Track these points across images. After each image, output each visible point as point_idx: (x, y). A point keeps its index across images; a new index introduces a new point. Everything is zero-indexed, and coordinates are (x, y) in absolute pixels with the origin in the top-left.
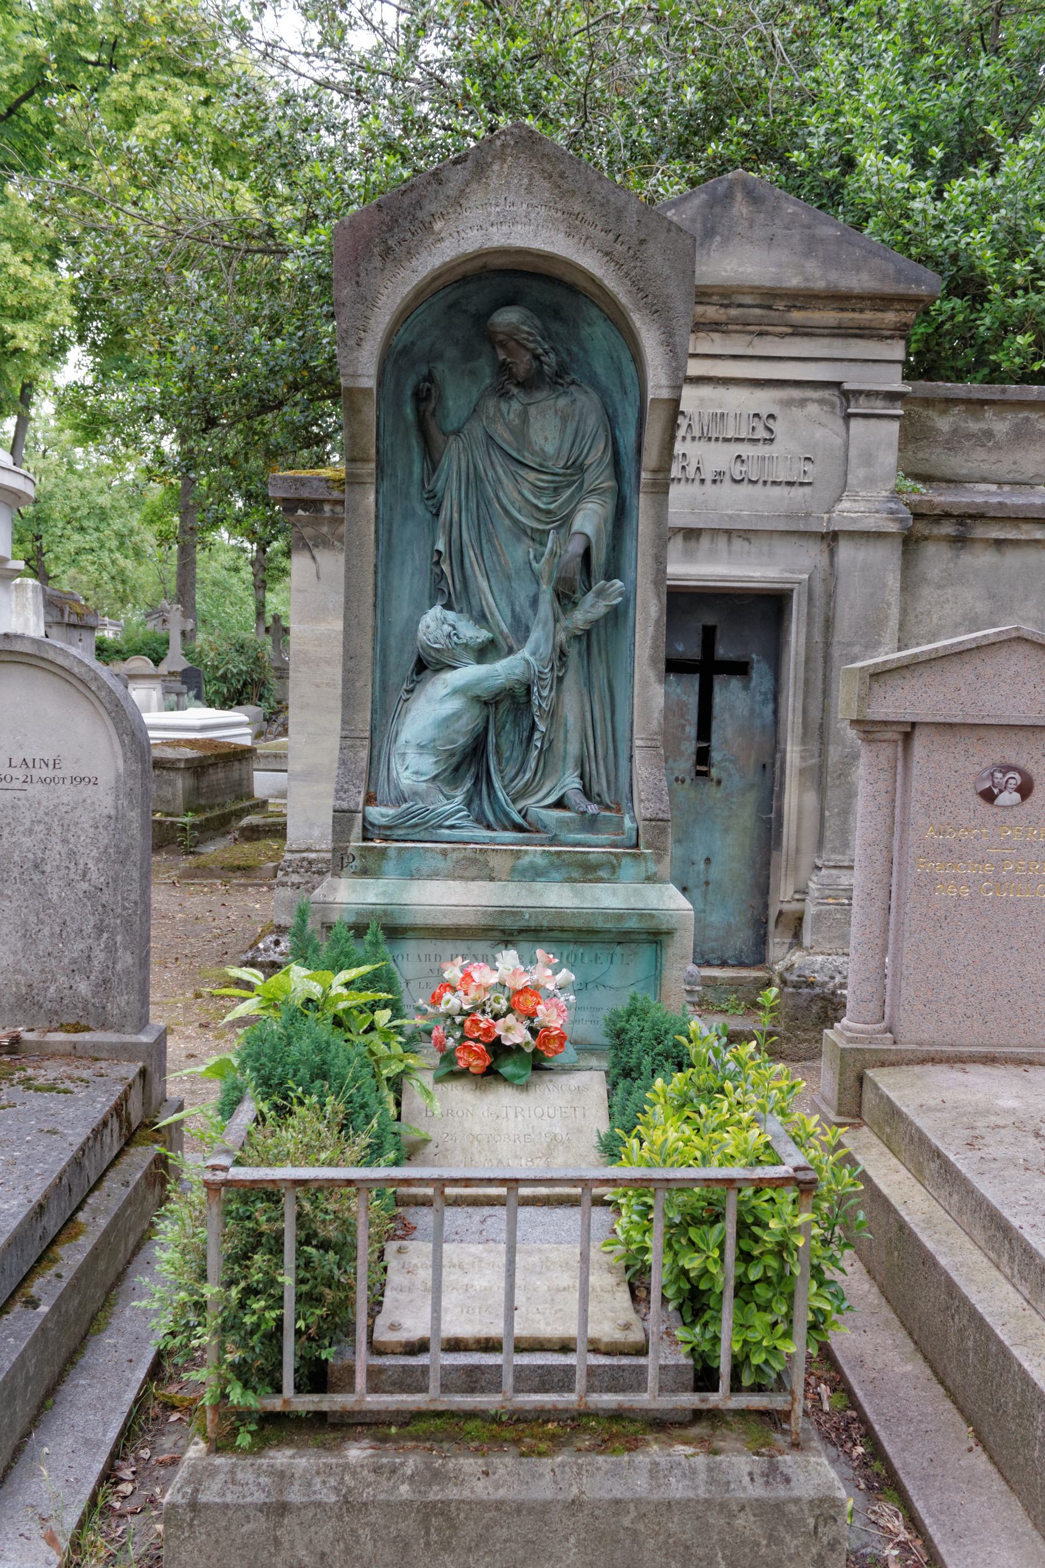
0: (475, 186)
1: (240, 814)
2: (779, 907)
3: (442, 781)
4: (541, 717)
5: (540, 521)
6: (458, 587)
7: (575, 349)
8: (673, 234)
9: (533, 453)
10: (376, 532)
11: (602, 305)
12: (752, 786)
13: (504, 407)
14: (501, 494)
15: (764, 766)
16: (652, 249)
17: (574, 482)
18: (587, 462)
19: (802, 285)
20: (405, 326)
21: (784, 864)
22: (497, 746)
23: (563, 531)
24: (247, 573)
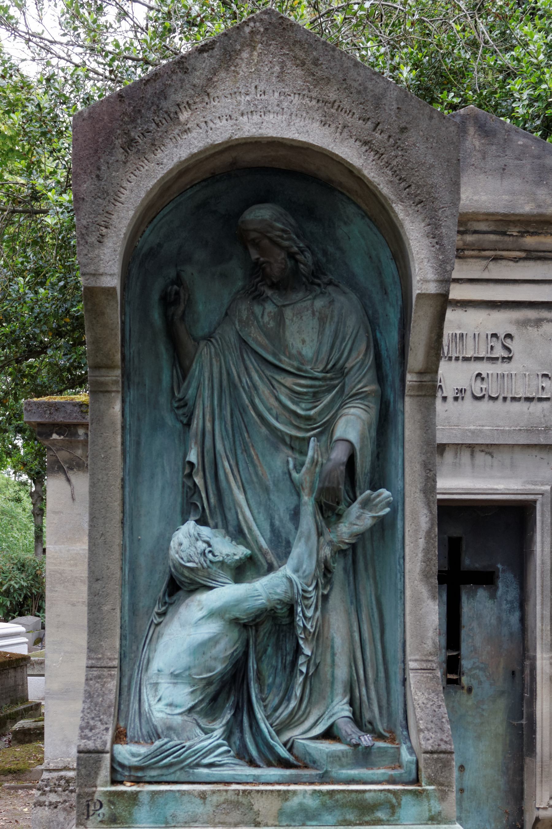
0: (223, 74)
1: (15, 717)
2: (536, 813)
3: (198, 713)
4: (305, 640)
5: (298, 428)
6: (212, 500)
7: (331, 249)
8: (436, 121)
9: (290, 357)
10: (123, 443)
11: (359, 201)
12: (502, 693)
13: (257, 309)
14: (257, 401)
15: (513, 673)
16: (413, 137)
17: (335, 387)
18: (348, 365)
19: (535, 211)
20: (151, 227)
21: (538, 770)
22: (259, 672)
23: (324, 438)
24: (28, 503)
